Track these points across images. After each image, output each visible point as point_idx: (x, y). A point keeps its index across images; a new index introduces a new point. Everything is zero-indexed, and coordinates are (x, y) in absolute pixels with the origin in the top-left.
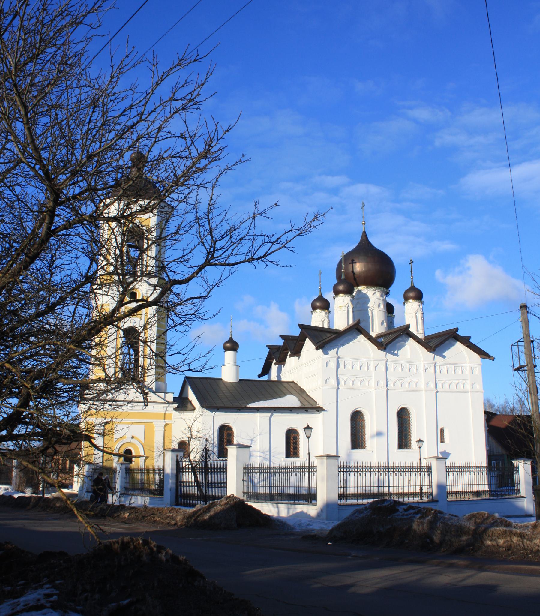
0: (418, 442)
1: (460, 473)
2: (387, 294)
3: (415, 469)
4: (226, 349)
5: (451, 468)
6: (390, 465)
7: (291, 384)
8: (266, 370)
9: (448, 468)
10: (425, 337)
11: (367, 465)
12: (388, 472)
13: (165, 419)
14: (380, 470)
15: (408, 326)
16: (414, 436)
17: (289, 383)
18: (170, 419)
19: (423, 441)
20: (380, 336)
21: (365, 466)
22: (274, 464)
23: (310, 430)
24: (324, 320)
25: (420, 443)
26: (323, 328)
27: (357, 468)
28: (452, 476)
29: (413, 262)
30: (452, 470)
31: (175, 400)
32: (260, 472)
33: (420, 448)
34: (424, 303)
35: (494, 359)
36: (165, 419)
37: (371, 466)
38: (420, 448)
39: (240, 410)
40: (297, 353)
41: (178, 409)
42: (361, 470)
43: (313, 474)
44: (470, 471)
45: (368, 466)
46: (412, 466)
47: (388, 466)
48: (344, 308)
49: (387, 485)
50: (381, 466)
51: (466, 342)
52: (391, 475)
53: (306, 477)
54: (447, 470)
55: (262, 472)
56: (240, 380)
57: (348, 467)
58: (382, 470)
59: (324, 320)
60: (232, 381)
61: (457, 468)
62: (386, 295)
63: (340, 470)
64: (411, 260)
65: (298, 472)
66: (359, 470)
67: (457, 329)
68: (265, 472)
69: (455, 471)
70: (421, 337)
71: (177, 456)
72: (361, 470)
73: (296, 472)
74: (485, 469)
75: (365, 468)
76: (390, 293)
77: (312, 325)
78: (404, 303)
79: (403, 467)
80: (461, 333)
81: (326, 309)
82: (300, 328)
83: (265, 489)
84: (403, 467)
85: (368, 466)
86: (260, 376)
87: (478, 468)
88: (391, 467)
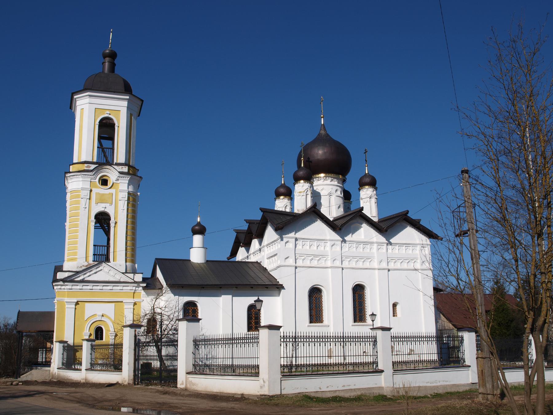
0: (371, 316)
1: (251, 345)
2: (344, 181)
3: (360, 338)
4: (195, 232)
5: (396, 338)
6: (344, 335)
7: (256, 265)
8: (234, 253)
9: (394, 338)
10: (379, 220)
11: (310, 335)
12: (343, 341)
13: (134, 298)
14: (324, 340)
15: (362, 209)
16: (369, 311)
17: (254, 264)
18: (140, 297)
19: (376, 315)
20: (336, 219)
21: (309, 336)
22: (222, 336)
23: (261, 303)
24: (287, 206)
25: (373, 317)
26: (285, 212)
27: (312, 338)
28: (240, 348)
29: (367, 151)
30: (414, 339)
31: (144, 280)
32: (204, 344)
33: (373, 321)
34: (378, 189)
35: (336, 196)
36: (134, 298)
37: (338, 336)
38: (373, 321)
39: (252, 288)
40: (260, 236)
41: (146, 288)
42: (305, 340)
43: (236, 345)
44: (419, 341)
45: (312, 336)
46: (418, 335)
47: (295, 336)
48: (303, 193)
49: (234, 359)
50: (372, 336)
51: (417, 225)
52: (346, 345)
53: (230, 348)
54: (393, 339)
55: (206, 344)
56: (207, 261)
57: (291, 337)
58: (326, 340)
59: (287, 206)
60: (199, 262)
61: (402, 338)
62: (343, 182)
63: (282, 340)
64: (365, 150)
65: (251, 342)
66: (313, 340)
67: (407, 212)
68: (227, 343)
69: (400, 341)
70: (376, 220)
71: (135, 331)
72: (316, 340)
73: (241, 343)
74: (435, 339)
75: (320, 338)
76: (347, 180)
77: (276, 209)
78: (360, 190)
79: (353, 337)
80: (412, 215)
81: (288, 196)
82: (262, 212)
83: (398, 349)
84: (348, 336)
85: (312, 336)
86: (228, 259)
87: (427, 338)
88: (346, 336)
